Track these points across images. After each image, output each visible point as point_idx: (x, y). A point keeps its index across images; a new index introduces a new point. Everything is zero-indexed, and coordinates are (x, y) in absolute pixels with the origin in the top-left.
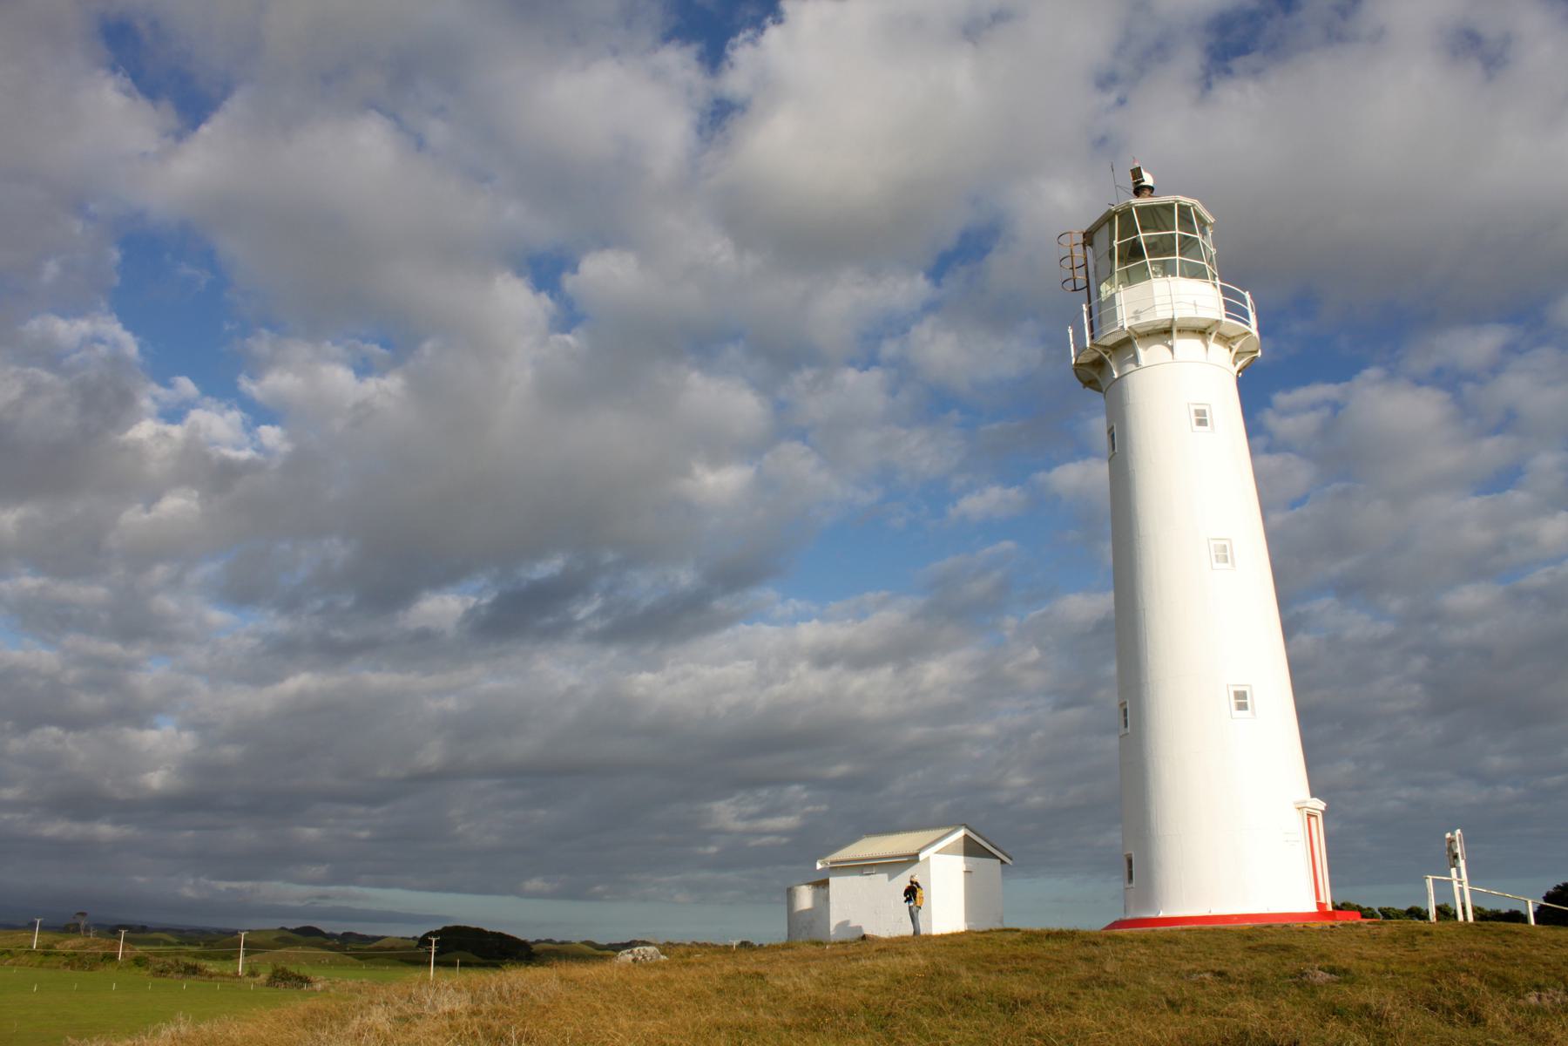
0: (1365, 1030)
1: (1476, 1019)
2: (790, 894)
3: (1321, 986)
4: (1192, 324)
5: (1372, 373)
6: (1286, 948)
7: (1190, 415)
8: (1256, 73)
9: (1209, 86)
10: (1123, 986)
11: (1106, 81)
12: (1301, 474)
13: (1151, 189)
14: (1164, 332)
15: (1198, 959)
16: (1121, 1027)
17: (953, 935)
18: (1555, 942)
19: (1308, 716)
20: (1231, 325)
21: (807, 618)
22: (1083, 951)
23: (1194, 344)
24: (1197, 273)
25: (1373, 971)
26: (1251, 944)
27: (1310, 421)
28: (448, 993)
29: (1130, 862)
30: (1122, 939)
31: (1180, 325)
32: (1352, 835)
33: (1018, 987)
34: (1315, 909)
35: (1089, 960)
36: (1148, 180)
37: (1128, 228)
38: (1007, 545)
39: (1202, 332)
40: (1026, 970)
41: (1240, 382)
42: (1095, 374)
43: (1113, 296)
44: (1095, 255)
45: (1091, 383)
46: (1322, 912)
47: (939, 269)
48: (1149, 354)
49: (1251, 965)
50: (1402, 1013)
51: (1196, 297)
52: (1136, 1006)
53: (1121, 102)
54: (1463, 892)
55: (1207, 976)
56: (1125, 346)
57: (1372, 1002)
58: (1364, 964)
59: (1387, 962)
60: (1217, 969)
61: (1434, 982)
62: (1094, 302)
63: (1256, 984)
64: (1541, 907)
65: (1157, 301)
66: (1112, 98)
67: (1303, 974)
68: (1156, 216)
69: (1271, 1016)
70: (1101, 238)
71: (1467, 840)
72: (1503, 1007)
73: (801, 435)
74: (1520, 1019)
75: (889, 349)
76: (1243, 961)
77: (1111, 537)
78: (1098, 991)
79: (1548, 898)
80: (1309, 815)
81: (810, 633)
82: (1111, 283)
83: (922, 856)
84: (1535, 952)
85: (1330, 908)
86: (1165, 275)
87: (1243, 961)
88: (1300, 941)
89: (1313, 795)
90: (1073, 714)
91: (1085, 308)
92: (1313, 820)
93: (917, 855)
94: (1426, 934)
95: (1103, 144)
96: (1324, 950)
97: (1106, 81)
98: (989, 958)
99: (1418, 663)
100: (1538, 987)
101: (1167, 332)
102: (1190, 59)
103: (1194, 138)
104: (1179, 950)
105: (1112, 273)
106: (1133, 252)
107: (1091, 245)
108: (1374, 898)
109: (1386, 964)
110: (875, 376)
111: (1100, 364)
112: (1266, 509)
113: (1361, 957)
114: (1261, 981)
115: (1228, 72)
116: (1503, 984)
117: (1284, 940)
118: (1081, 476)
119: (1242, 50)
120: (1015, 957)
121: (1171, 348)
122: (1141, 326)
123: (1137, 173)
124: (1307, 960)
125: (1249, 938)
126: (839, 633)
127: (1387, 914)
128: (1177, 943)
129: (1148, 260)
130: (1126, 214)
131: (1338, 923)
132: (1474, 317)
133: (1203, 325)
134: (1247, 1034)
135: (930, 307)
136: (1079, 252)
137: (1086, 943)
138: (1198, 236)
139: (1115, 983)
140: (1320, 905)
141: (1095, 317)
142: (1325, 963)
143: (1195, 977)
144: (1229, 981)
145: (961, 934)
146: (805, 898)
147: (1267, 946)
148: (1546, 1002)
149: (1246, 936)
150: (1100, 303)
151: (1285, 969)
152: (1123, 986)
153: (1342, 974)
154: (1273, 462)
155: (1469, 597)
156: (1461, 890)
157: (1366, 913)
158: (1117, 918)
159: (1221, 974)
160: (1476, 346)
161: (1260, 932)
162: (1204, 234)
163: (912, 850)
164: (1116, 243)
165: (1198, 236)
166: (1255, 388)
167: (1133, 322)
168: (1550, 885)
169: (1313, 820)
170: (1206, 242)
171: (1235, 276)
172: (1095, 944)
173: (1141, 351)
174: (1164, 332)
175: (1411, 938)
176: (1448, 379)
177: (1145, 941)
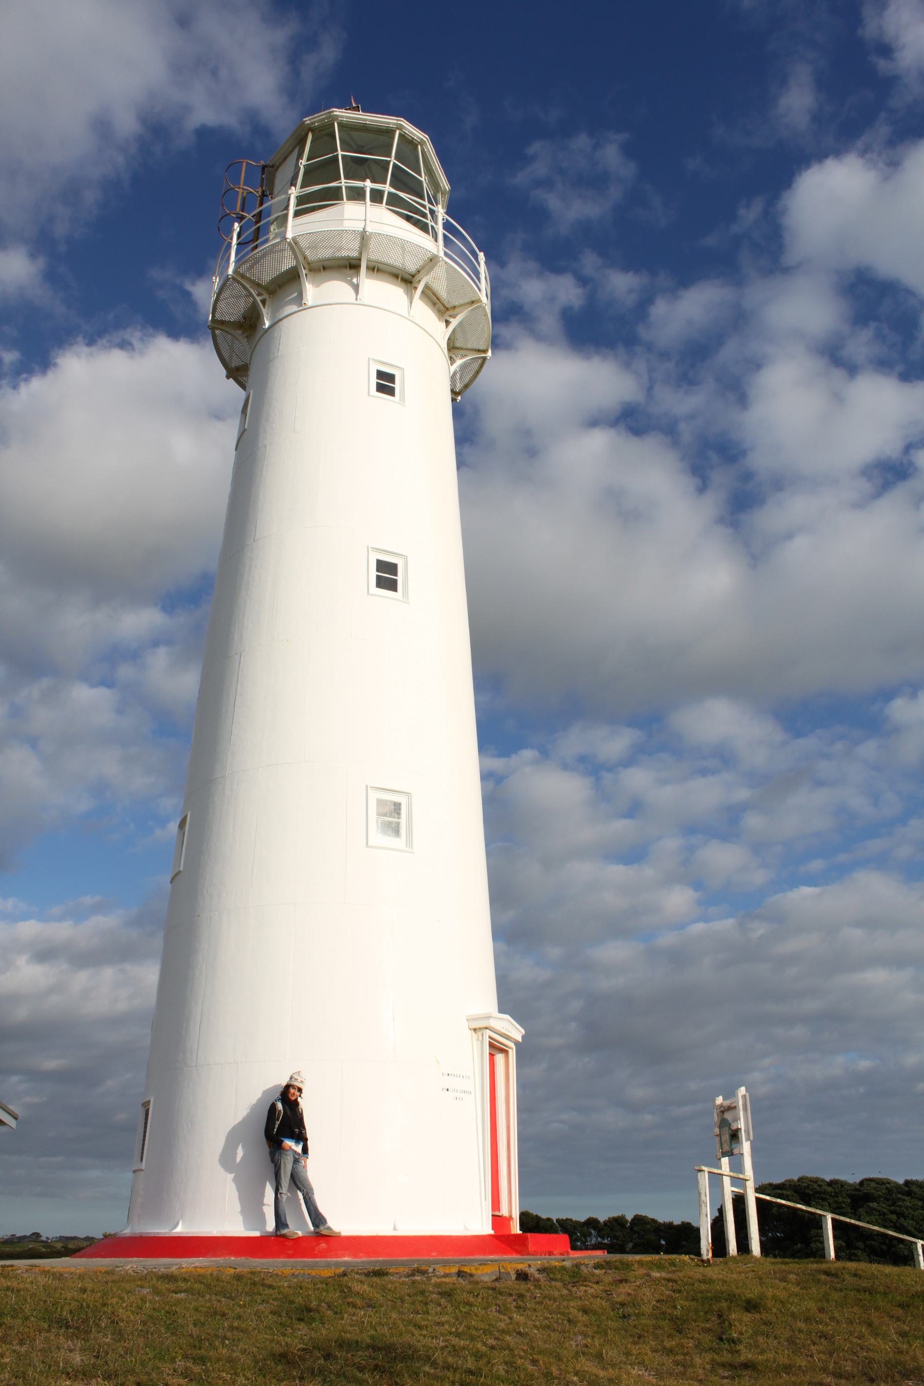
5: (528, 754)
21: (26, 917)
23: (394, 292)
34: (485, 1228)
46: (501, 1239)
56: (287, 284)
73: (33, 742)
75: (125, 672)
80: (496, 1048)
81: (29, 929)
85: (516, 1228)
92: (499, 1058)
101: (353, 266)
121: (356, 288)
125: (305, 1313)
126: (61, 931)
140: (499, 1221)
160: (614, 743)
169: (499, 1058)
176: (591, 767)
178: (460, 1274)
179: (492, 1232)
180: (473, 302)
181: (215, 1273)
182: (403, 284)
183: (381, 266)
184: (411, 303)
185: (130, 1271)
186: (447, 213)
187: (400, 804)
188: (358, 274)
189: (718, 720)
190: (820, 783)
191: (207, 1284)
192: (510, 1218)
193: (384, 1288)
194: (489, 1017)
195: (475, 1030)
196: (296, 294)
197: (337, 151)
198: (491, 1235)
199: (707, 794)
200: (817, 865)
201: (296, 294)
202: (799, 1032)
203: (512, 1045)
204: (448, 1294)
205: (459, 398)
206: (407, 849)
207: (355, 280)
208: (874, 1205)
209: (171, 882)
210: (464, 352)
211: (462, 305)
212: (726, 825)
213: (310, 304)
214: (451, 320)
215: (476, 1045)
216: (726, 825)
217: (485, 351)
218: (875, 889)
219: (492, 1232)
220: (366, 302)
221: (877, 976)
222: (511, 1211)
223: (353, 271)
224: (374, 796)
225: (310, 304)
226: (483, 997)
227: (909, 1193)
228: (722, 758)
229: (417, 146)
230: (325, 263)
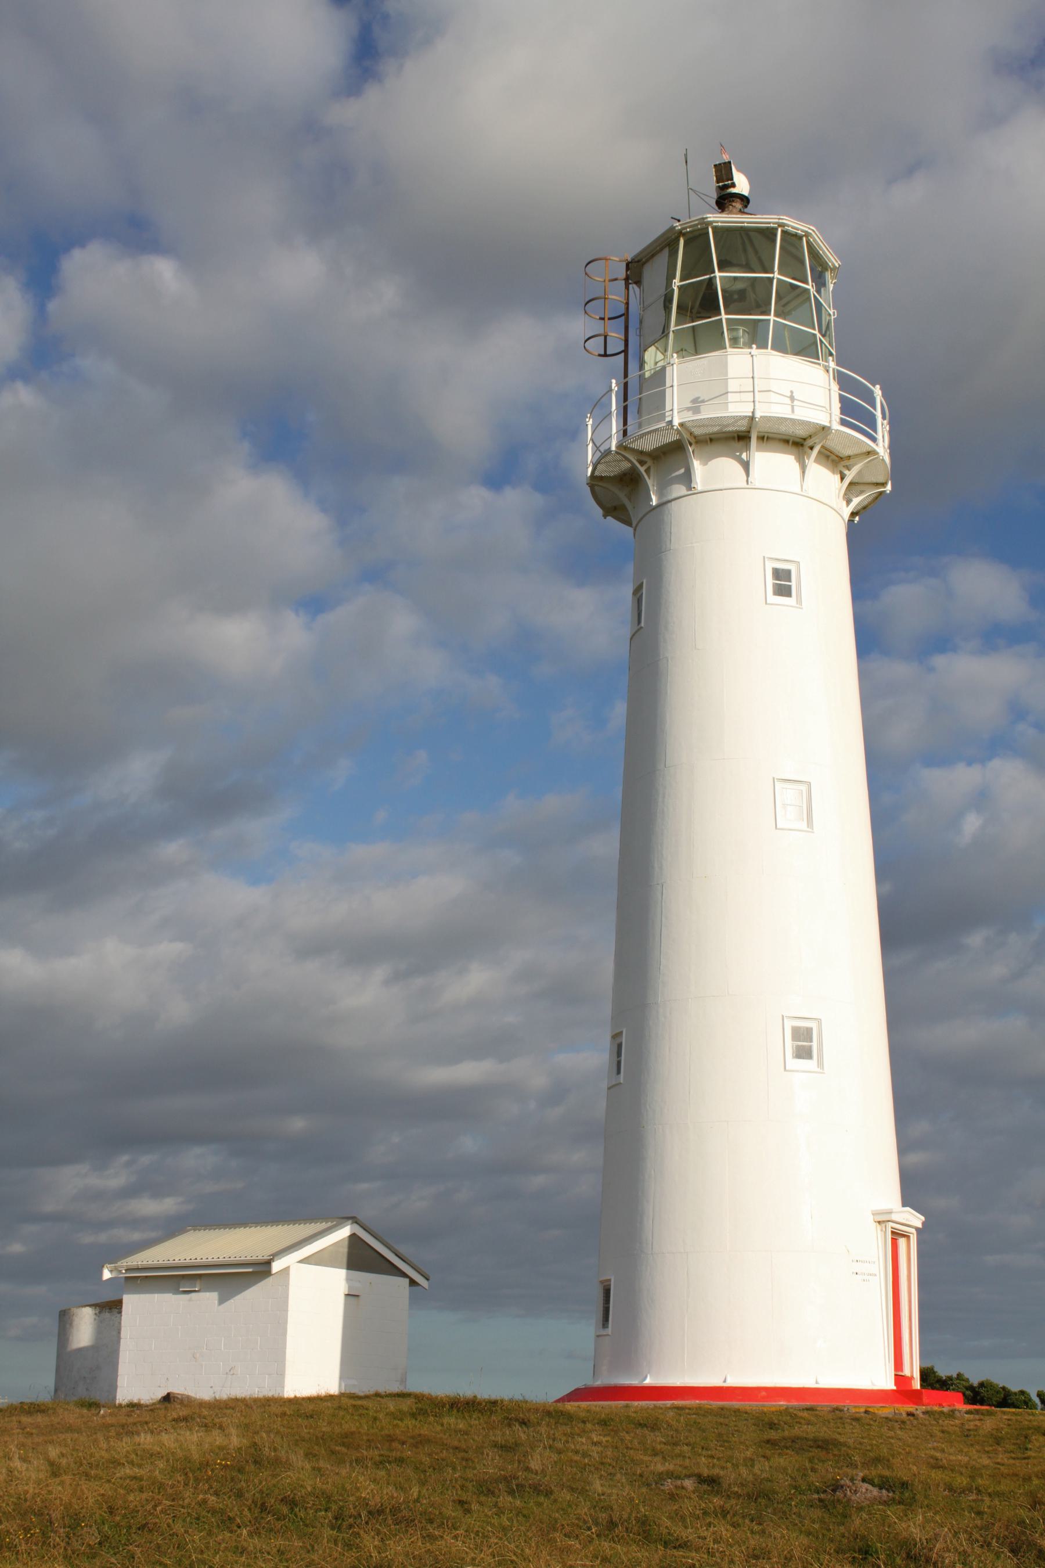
2: (65, 1319)
3: (860, 1509)
4: (783, 429)
6: (823, 1445)
10: (548, 1493)
13: (745, 200)
14: (737, 438)
17: (310, 1400)
22: (498, 1436)
24: (806, 349)
26: (773, 1435)
29: (607, 1292)
30: (569, 1417)
31: (764, 428)
33: (369, 1487)
34: (889, 1384)
35: (505, 1448)
36: (742, 184)
37: (698, 262)
39: (797, 442)
40: (400, 1461)
42: (622, 495)
43: (664, 368)
44: (642, 301)
45: (614, 510)
46: (902, 1390)
48: (710, 471)
49: (762, 1468)
51: (792, 385)
55: (689, 1483)
56: (673, 454)
58: (936, 1475)
59: (974, 1472)
60: (705, 1472)
62: (633, 373)
65: (732, 385)
67: (836, 1487)
68: (748, 246)
70: (654, 273)
76: (750, 1462)
80: (896, 1235)
83: (276, 1266)
85: (917, 1385)
87: (750, 1462)
88: (850, 1435)
89: (904, 1205)
92: (902, 1242)
93: (268, 1263)
98: (347, 1439)
106: (702, 303)
107: (638, 283)
109: (972, 1478)
110: (517, 500)
111: (631, 480)
113: (937, 1466)
117: (824, 1432)
120: (390, 1439)
121: (746, 466)
122: (701, 424)
123: (723, 172)
125: (772, 1425)
129: (724, 316)
130: (697, 238)
131: (919, 1410)
133: (801, 432)
136: (616, 295)
137: (509, 1422)
139: (536, 1489)
140: (900, 1379)
141: (632, 398)
143: (669, 1485)
145: (330, 1398)
146: (84, 1328)
149: (768, 1423)
152: (548, 1493)
153: (900, 1492)
158: (579, 1384)
162: (820, 283)
163: (261, 1255)
164: (676, 283)
165: (810, 286)
166: (876, 545)
167: (689, 417)
172: (523, 1423)
173: (697, 465)
174: (737, 438)
175: (1022, 1438)
177: (604, 1423)
178: (866, 1412)
179: (895, 1388)
180: (869, 453)
182: (794, 449)
183: (770, 435)
184: (804, 473)
186: (837, 365)
187: (811, 1029)
188: (748, 448)
191: (698, 1411)
192: (912, 1378)
193: (816, 1416)
194: (890, 1212)
195: (879, 1222)
196: (682, 471)
197: (714, 272)
198: (893, 1391)
201: (682, 471)
203: (913, 1231)
204: (857, 1420)
205: (857, 519)
206: (819, 1070)
207: (744, 456)
209: (609, 1088)
210: (862, 487)
211: (856, 455)
213: (700, 488)
214: (846, 472)
215: (880, 1234)
217: (884, 484)
219: (895, 1388)
220: (758, 485)
222: (912, 1372)
223: (741, 444)
224: (789, 1025)
225: (700, 488)
226: (886, 1192)
229: (800, 238)
230: (712, 436)
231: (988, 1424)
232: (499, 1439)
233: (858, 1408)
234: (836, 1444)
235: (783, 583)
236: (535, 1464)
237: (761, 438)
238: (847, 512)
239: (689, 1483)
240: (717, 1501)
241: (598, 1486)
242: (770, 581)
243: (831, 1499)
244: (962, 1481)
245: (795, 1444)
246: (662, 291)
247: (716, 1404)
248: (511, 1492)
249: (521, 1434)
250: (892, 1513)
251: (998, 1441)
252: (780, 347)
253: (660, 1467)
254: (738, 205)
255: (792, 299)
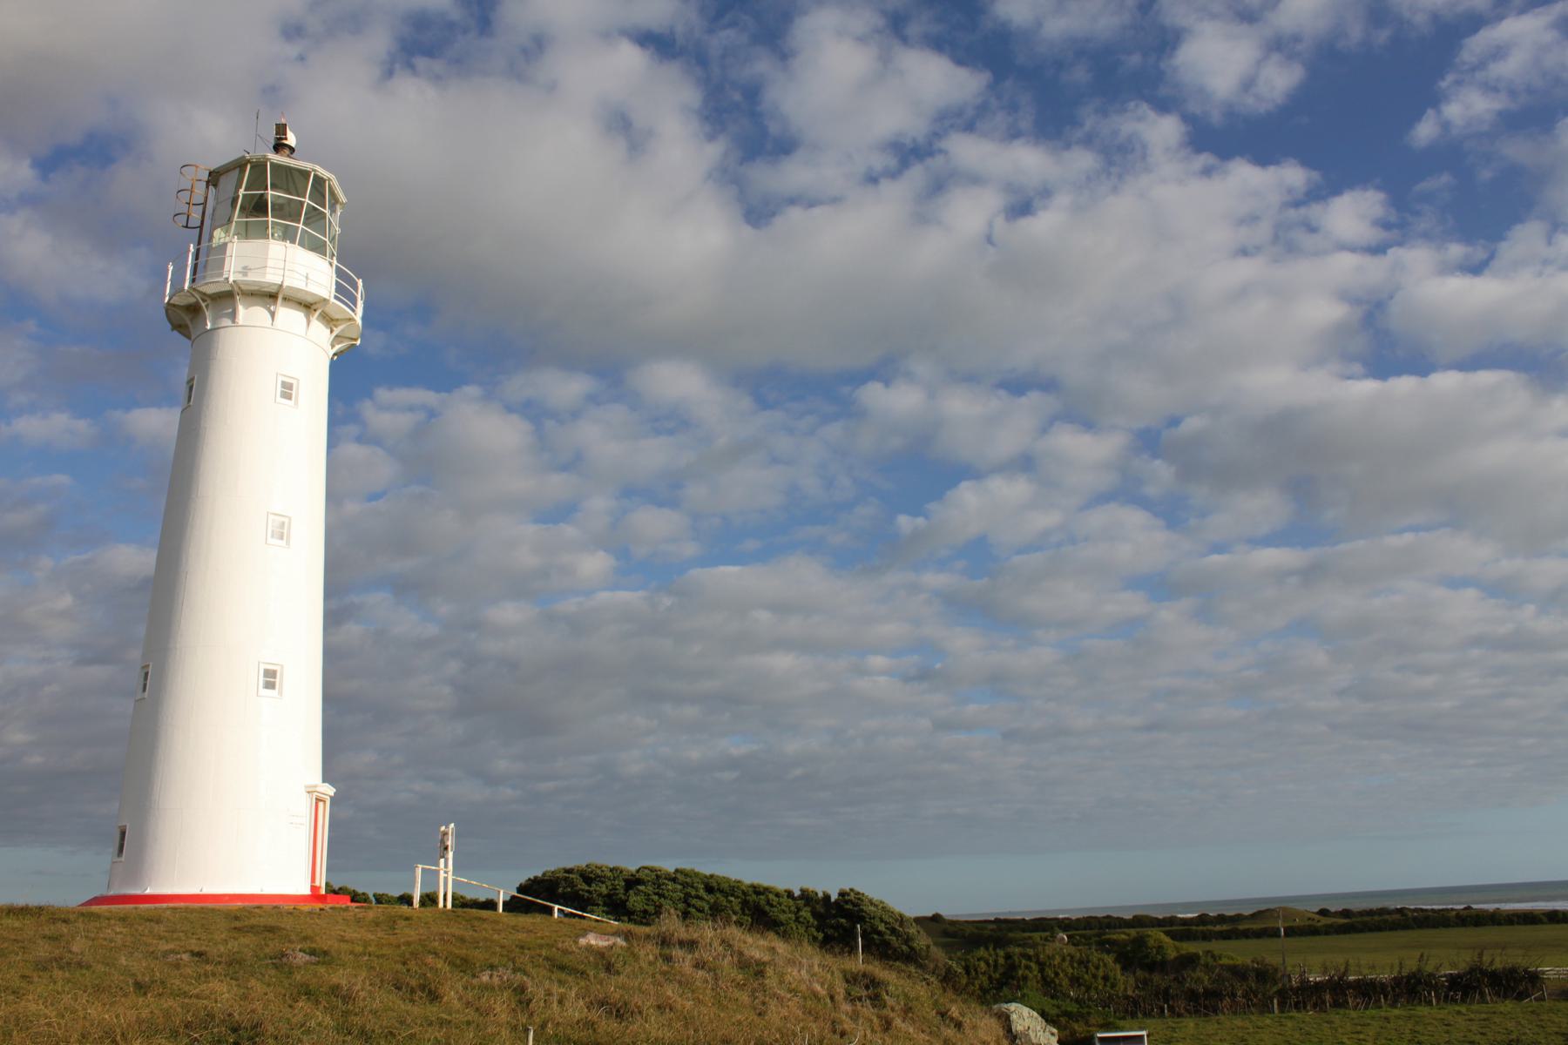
0: (330, 1009)
1: (434, 996)
3: (299, 967)
4: (299, 296)
5: (472, 390)
6: (271, 929)
7: (276, 385)
8: (437, 79)
9: (389, 73)
10: (88, 967)
11: (292, 31)
12: (383, 470)
13: (292, 150)
14: (269, 296)
15: (179, 939)
16: (74, 1011)
18: (513, 928)
19: (333, 701)
20: (339, 307)
23: (298, 316)
24: (317, 248)
25: (352, 953)
26: (237, 924)
27: (405, 421)
28: (1462, 1018)
29: (123, 834)
30: (98, 916)
31: (288, 293)
32: (350, 824)
34: (308, 892)
35: (54, 939)
36: (291, 139)
37: (258, 180)
38: (62, 479)
39: (307, 305)
41: (334, 367)
42: (187, 319)
43: (225, 244)
44: (216, 198)
45: (180, 328)
46: (315, 895)
47: (51, 163)
50: (370, 992)
51: (311, 271)
52: (99, 990)
53: (302, 58)
54: (447, 879)
56: (226, 299)
57: (344, 982)
58: (344, 946)
59: (366, 944)
61: (404, 963)
62: (204, 244)
63: (234, 965)
64: (513, 897)
65: (270, 263)
66: (293, 50)
67: (283, 955)
68: (290, 178)
69: (245, 997)
70: (227, 182)
71: (458, 835)
72: (459, 986)
74: (470, 995)
76: (226, 942)
77: (168, 496)
78: (58, 973)
79: (521, 889)
80: (318, 800)
82: (227, 232)
84: (496, 937)
85: (323, 892)
86: (284, 239)
87: (226, 942)
88: (287, 923)
90: (98, 673)
91: (192, 248)
94: (407, 919)
95: (272, 93)
96: (309, 932)
97: (292, 31)
99: (453, 667)
100: (492, 967)
102: (380, 41)
103: (355, 117)
104: (160, 929)
105: (230, 221)
106: (258, 207)
107: (215, 185)
108: (368, 884)
111: (194, 310)
112: (334, 497)
113: (342, 940)
114: (239, 962)
115: (411, 67)
116: (464, 965)
117: (271, 922)
118: (155, 422)
119: (430, 52)
121: (273, 314)
123: (281, 130)
124: (291, 942)
125: (237, 918)
127: (380, 899)
128: (158, 922)
130: (259, 167)
131: (327, 907)
132: (569, 362)
133: (310, 299)
134: (213, 1017)
135: (28, 200)
136: (200, 189)
138: (327, 211)
139: (80, 965)
140: (314, 888)
141: (202, 259)
142: (307, 945)
143: (172, 958)
144: (207, 962)
147: (252, 927)
148: (496, 980)
150: (210, 248)
151: (267, 950)
152: (88, 967)
153: (322, 956)
154: (352, 450)
155: (509, 613)
156: (446, 879)
157: (355, 897)
158: (98, 894)
159: (199, 954)
160: (566, 388)
161: (249, 913)
162: (333, 211)
164: (242, 192)
166: (350, 379)
167: (240, 277)
168: (523, 877)
170: (334, 219)
171: (355, 262)
172: (65, 921)
173: (241, 309)
174: (269, 296)
175: (392, 922)
176: (534, 412)
177: (123, 919)
181: (834, 897)
185: (1151, 943)
188: (275, 303)
189: (677, 382)
190: (775, 460)
199: (655, 455)
200: (751, 545)
202: (690, 711)
208: (642, 888)
212: (662, 492)
216: (662, 492)
218: (803, 576)
221: (782, 662)
227: (674, 880)
228: (671, 421)
231: (371, 915)
232: (47, 932)
233: (289, 907)
234: (280, 929)
235: (287, 391)
236: (75, 949)
237: (285, 299)
238: (332, 352)
239: (185, 957)
240: (209, 968)
241: (123, 961)
242: (279, 389)
243: (280, 962)
244: (359, 949)
245: (252, 929)
246: (232, 195)
247: (197, 905)
248: (61, 968)
249: (64, 929)
250: (322, 970)
251: (377, 925)
252: (301, 244)
253: (164, 946)
254: (287, 151)
255: (315, 217)
